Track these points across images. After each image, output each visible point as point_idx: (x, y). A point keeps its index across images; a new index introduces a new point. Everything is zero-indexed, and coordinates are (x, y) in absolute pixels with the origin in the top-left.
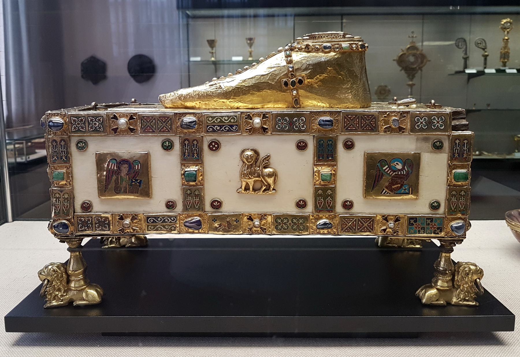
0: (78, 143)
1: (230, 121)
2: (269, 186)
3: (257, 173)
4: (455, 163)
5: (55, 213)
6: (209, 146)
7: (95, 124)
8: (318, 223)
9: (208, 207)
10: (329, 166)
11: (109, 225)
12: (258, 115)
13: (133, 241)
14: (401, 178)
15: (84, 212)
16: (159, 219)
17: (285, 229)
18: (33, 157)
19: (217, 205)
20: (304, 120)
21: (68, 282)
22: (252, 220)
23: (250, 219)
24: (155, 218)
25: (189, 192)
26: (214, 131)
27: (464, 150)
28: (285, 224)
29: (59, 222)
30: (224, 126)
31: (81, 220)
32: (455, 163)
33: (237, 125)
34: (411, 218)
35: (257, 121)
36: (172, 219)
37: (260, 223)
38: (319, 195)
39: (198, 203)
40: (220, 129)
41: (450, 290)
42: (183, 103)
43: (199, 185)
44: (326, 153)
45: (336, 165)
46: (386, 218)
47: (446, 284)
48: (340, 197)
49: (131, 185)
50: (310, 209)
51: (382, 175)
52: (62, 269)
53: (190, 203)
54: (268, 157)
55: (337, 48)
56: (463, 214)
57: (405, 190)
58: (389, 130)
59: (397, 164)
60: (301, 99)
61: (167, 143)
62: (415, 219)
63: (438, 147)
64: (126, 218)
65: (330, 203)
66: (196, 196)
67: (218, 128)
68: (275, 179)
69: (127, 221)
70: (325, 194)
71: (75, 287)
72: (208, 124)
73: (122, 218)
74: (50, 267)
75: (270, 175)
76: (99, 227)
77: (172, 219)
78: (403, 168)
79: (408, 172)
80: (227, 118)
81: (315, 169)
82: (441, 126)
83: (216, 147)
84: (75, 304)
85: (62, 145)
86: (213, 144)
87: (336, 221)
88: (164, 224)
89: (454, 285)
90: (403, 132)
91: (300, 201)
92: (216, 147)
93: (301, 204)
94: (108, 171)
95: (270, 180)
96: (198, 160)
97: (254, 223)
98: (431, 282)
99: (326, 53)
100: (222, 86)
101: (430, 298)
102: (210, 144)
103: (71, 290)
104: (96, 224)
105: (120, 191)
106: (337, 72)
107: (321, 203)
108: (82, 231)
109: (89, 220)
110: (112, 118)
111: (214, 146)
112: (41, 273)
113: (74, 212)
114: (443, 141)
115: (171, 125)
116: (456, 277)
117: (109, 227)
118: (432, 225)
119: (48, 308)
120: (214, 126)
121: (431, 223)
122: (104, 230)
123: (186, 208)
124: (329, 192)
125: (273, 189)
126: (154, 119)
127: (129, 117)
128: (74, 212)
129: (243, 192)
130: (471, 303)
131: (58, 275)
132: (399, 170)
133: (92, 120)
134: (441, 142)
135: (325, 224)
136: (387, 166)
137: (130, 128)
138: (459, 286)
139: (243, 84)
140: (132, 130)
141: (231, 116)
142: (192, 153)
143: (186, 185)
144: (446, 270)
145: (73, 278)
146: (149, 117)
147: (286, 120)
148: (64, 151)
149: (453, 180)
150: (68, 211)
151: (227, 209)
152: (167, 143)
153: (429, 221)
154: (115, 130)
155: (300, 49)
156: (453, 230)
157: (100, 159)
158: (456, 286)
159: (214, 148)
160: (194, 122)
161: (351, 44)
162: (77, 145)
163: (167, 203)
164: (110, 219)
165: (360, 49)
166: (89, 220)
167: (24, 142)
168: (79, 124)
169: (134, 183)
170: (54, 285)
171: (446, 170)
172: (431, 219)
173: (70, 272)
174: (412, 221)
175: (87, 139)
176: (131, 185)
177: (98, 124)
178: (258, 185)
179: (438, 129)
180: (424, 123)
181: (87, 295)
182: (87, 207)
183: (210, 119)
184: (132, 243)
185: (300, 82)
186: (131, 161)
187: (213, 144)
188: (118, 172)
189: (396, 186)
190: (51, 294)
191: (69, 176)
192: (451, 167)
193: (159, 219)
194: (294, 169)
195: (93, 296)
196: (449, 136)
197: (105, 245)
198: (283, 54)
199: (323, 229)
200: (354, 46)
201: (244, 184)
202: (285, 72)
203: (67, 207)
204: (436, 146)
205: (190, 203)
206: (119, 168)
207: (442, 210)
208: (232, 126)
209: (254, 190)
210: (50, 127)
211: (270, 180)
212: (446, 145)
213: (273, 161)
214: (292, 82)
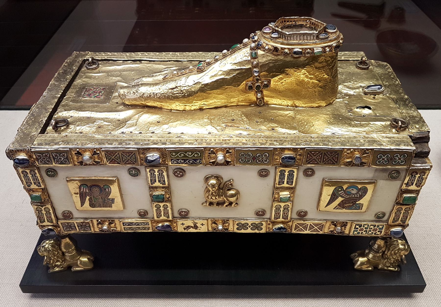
1: (194, 156)
30: (187, 160)
33: (201, 159)
35: (220, 157)
40: (184, 162)
58: (350, 164)
61: (133, 171)
68: (237, 198)
75: (232, 196)
86: (178, 172)
95: (232, 199)
120: (178, 160)
133: (56, 156)
152: (133, 171)
154: (81, 163)
159: (179, 176)
161: (324, 48)
171: (398, 192)
177: (63, 159)
180: (385, 159)
183: (174, 154)
187: (178, 172)
200: (328, 49)
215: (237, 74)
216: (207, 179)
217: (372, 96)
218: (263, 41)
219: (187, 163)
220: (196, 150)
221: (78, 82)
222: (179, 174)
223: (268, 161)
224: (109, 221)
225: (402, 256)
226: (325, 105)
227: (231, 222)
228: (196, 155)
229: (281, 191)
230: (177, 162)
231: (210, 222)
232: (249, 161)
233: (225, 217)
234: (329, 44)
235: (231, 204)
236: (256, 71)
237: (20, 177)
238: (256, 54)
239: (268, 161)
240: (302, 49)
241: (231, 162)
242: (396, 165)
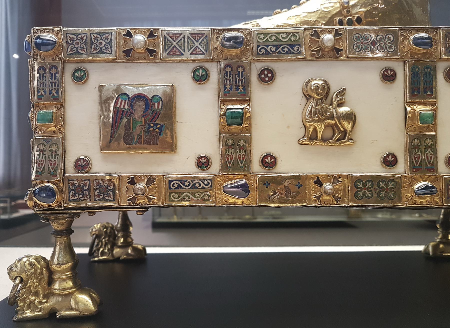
0: (76, 71)
2: (345, 132)
5: (37, 172)
6: (260, 76)
7: (101, 43)
9: (256, 167)
10: (425, 104)
13: (130, 251)
15: (79, 173)
16: (187, 184)
17: (368, 197)
18: (15, 215)
19: (269, 161)
20: (392, 38)
21: (51, 282)
23: (319, 182)
24: (180, 181)
25: (230, 142)
26: (267, 53)
28: (368, 189)
30: (281, 45)
31: (73, 185)
33: (299, 45)
36: (206, 182)
39: (243, 159)
40: (276, 49)
45: (435, 103)
49: (148, 132)
50: (401, 168)
53: (231, 159)
54: (342, 92)
61: (201, 71)
65: (431, 158)
66: (242, 148)
67: (273, 49)
69: (141, 185)
71: (59, 289)
72: (259, 44)
74: (25, 259)
76: (99, 195)
77: (206, 182)
80: (285, 36)
83: (269, 78)
84: (58, 315)
85: (52, 74)
86: (266, 72)
87: (441, 185)
88: (194, 190)
91: (388, 155)
92: (269, 78)
93: (390, 161)
94: (116, 111)
96: (245, 95)
102: (262, 72)
103: (53, 294)
104: (95, 190)
105: (132, 140)
108: (74, 200)
109: (85, 185)
111: (267, 76)
112: (11, 269)
119: (19, 321)
120: (268, 46)
123: (225, 168)
124: (429, 142)
127: (147, 34)
128: (64, 173)
131: (36, 271)
133: (96, 38)
135: (426, 188)
140: (151, 52)
141: (290, 33)
142: (235, 87)
145: (57, 276)
146: (176, 34)
150: (56, 170)
151: (284, 168)
162: (74, 74)
163: (199, 159)
166: (85, 185)
167: (8, 200)
168: (77, 43)
169: (151, 129)
170: (30, 287)
175: (88, 66)
176: (148, 132)
177: (104, 43)
181: (77, 303)
182: (83, 165)
183: (262, 36)
184: (128, 254)
187: (266, 72)
188: (130, 113)
190: (24, 300)
191: (60, 121)
193: (187, 184)
197: (95, 257)
202: (339, 9)
203: (55, 164)
205: (231, 159)
206: (131, 105)
208: (292, 46)
211: (348, 126)
213: (348, 96)
214: (348, 20)
222: (267, 76)
223: (393, 47)
228: (293, 39)
230: (266, 50)
237: (128, 62)
239: (393, 47)
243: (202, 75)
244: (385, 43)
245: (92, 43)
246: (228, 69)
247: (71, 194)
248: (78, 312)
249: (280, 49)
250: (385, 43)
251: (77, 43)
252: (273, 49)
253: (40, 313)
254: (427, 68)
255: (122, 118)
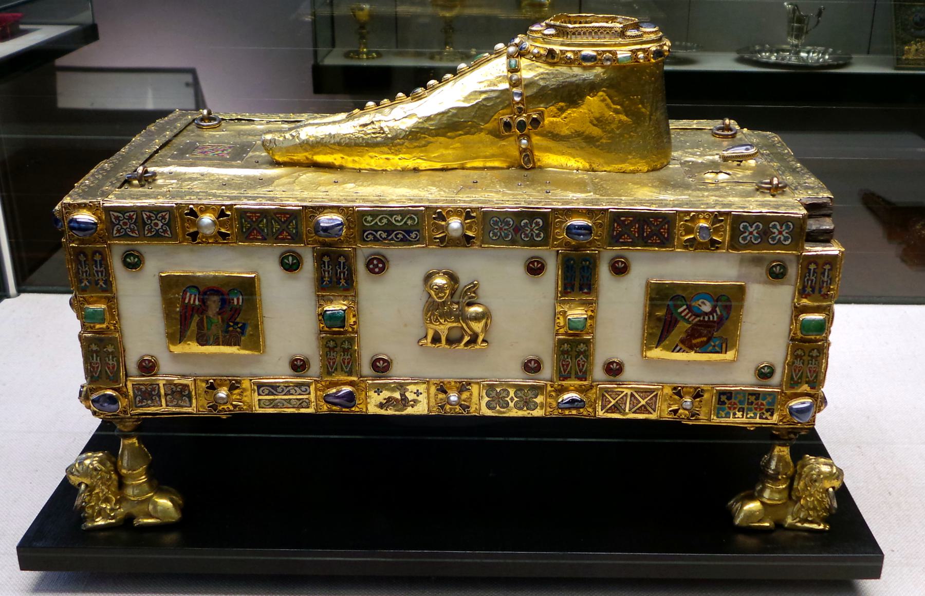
1: (405, 223)
3: (453, 313)
4: (805, 301)
6: (367, 266)
7: (156, 225)
8: (560, 400)
11: (189, 397)
12: (457, 212)
14: (708, 327)
15: (144, 376)
20: (541, 223)
22: (446, 392)
25: (332, 344)
26: (376, 240)
27: (823, 282)
29: (102, 392)
32: (805, 301)
33: (418, 231)
34: (721, 393)
35: (455, 223)
37: (459, 398)
38: (564, 352)
39: (348, 363)
40: (388, 236)
41: (784, 504)
42: (310, 157)
43: (350, 332)
44: (578, 279)
45: (596, 302)
46: (678, 392)
47: (777, 496)
48: (602, 354)
51: (676, 322)
52: (109, 464)
53: (334, 363)
54: (474, 288)
55: (608, 60)
56: (812, 388)
57: (714, 346)
58: (692, 244)
59: (703, 303)
60: (536, 153)
61: (290, 258)
62: (729, 395)
63: (777, 274)
64: (221, 385)
65: (583, 366)
66: (345, 351)
68: (486, 324)
69: (223, 393)
70: (574, 350)
73: (212, 387)
75: (477, 318)
76: (172, 402)
78: (713, 310)
79: (721, 318)
80: (399, 218)
81: (559, 309)
82: (786, 239)
83: (380, 269)
84: (136, 523)
85: (96, 261)
86: (375, 262)
89: (791, 495)
90: (717, 248)
92: (380, 269)
95: (478, 327)
97: (448, 398)
98: (753, 488)
99: (585, 68)
100: (386, 129)
101: (751, 514)
106: (607, 105)
107: (568, 365)
108: (142, 407)
110: (187, 214)
111: (377, 266)
113: (127, 376)
114: (788, 263)
115: (296, 228)
116: (795, 483)
117: (190, 401)
118: (757, 404)
120: (376, 232)
121: (755, 402)
122: (182, 407)
124: (582, 347)
125: (484, 341)
126: (266, 217)
129: (430, 345)
130: (815, 526)
132: (706, 314)
133: (149, 218)
134: (784, 268)
135: (573, 401)
136: (685, 307)
137: (220, 233)
138: (799, 499)
139: (426, 125)
140: (224, 236)
142: (335, 275)
143: (326, 332)
144: (778, 474)
147: (508, 224)
148: (102, 272)
149: (798, 332)
152: (290, 258)
153: (752, 398)
154: (194, 236)
155: (537, 57)
156: (791, 413)
157: (168, 284)
158: (794, 498)
159: (377, 270)
160: (339, 225)
161: (634, 52)
164: (192, 387)
165: (653, 61)
168: (125, 224)
169: (231, 329)
171: (789, 312)
172: (757, 395)
173: (124, 471)
174: (723, 398)
175: (143, 250)
177: (160, 224)
178: (456, 334)
179: (779, 245)
180: (755, 233)
183: (369, 218)
185: (536, 122)
186: (225, 290)
187: (375, 262)
188: (202, 309)
189: (699, 340)
192: (799, 310)
194: (519, 305)
195: (165, 510)
196: (798, 257)
198: (503, 59)
199: (569, 408)
200: (641, 55)
201: (430, 334)
203: (113, 368)
204: (774, 273)
205: (334, 363)
206: (203, 302)
207: (777, 378)
209: (450, 341)
210: (72, 228)
211: (478, 327)
212: (793, 271)
215: (485, 99)
216: (428, 277)
217: (736, 163)
218: (527, 44)
219: (392, 239)
220: (409, 212)
221: (184, 139)
222: (377, 266)
223: (542, 235)
224: (230, 381)
225: (827, 490)
226: (646, 169)
227: (475, 389)
229: (570, 309)
230: (375, 237)
231: (433, 390)
232: (507, 236)
233: (463, 376)
234: (644, 46)
235: (473, 340)
236: (516, 94)
238: (518, 64)
239: (542, 235)
240: (597, 51)
241: (473, 238)
242: (773, 247)
243: (293, 264)
244: (532, 230)
245: (145, 224)
246: (326, 259)
247: (138, 399)
248: (158, 520)
249: (393, 235)
250: (532, 230)
251: (125, 224)
252: (384, 235)
253: (113, 521)
254: (586, 260)
255: (192, 316)
